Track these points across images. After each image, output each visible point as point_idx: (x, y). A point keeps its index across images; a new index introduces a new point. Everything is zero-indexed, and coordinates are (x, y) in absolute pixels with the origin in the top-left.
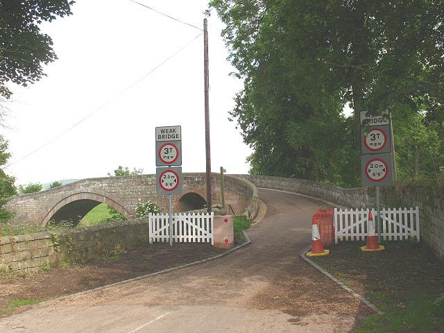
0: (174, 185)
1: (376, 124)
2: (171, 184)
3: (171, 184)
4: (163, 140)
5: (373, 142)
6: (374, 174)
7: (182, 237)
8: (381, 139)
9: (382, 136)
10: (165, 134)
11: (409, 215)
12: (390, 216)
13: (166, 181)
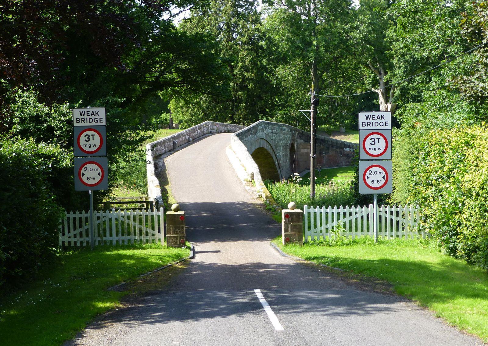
0: (383, 181)
1: (376, 128)
2: (378, 182)
3: (378, 182)
4: (369, 128)
5: (373, 147)
6: (88, 179)
7: (117, 238)
8: (382, 144)
9: (382, 140)
10: (85, 117)
11: (315, 213)
12: (395, 213)
13: (372, 177)
